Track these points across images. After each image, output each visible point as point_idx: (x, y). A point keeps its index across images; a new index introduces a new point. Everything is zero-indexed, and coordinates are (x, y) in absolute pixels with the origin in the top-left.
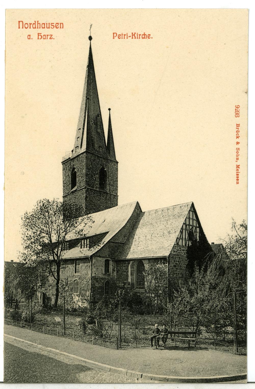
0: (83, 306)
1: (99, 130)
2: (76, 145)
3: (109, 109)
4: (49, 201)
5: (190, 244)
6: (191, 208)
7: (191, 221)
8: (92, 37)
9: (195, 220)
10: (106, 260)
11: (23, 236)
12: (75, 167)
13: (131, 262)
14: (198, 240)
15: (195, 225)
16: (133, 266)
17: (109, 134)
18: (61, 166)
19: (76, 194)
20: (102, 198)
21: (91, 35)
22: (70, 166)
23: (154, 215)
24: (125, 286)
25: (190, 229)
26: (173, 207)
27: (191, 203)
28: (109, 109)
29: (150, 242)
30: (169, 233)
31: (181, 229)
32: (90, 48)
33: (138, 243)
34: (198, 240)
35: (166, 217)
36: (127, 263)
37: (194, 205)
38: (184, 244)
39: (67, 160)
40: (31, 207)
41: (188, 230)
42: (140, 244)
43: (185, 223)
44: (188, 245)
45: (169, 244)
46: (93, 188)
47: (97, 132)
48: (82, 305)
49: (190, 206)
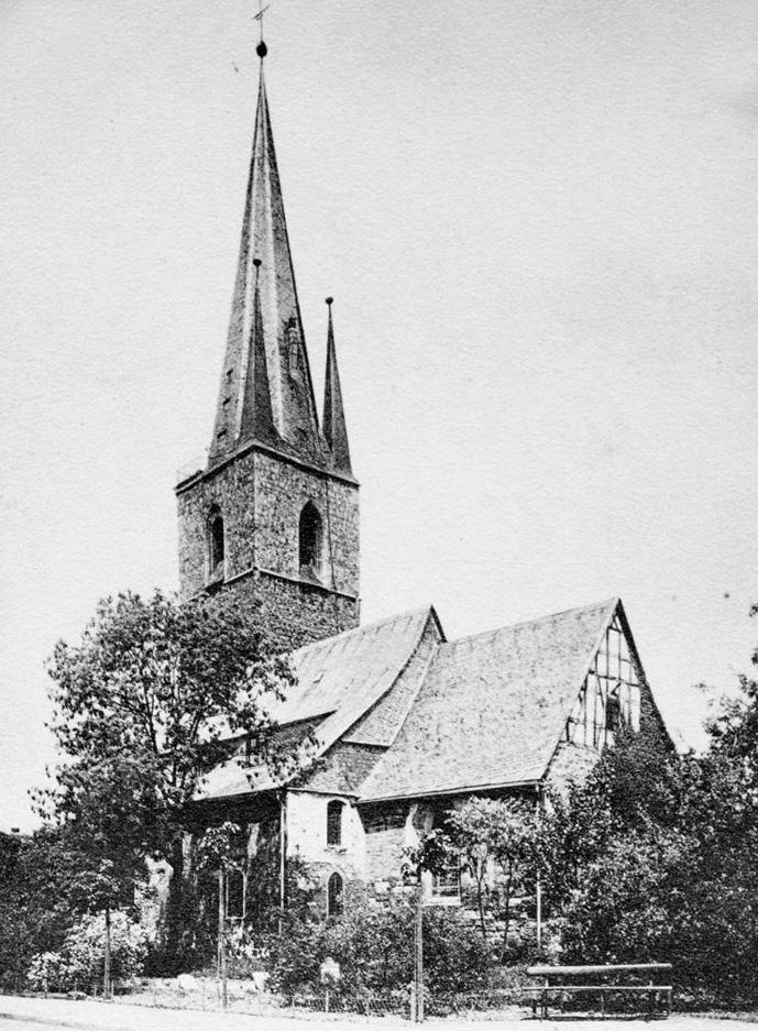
0: (259, 956)
1: (295, 374)
2: (220, 428)
3: (329, 301)
4: (142, 600)
5: (611, 742)
6: (614, 620)
7: (614, 662)
8: (268, 45)
9: (625, 660)
10: (329, 804)
11: (54, 684)
12: (218, 500)
13: (413, 810)
14: (669, 965)
15: (625, 677)
16: (420, 820)
17: (328, 393)
18: (174, 502)
19: (224, 595)
20: (310, 606)
21: (259, 58)
22: (201, 500)
23: (488, 649)
24: (396, 890)
25: (610, 690)
26: (550, 619)
27: (615, 602)
28: (329, 301)
29: (474, 739)
30: (541, 704)
31: (582, 689)
32: (266, 155)
33: (437, 742)
34: (669, 965)
35: (531, 654)
36: (400, 811)
37: (622, 609)
38: (590, 742)
39: (192, 478)
40: (79, 629)
41: (604, 695)
42: (442, 745)
43: (593, 669)
44: (606, 744)
45: (542, 741)
46: (279, 571)
47: (290, 379)
48: (255, 953)
49: (612, 611)
